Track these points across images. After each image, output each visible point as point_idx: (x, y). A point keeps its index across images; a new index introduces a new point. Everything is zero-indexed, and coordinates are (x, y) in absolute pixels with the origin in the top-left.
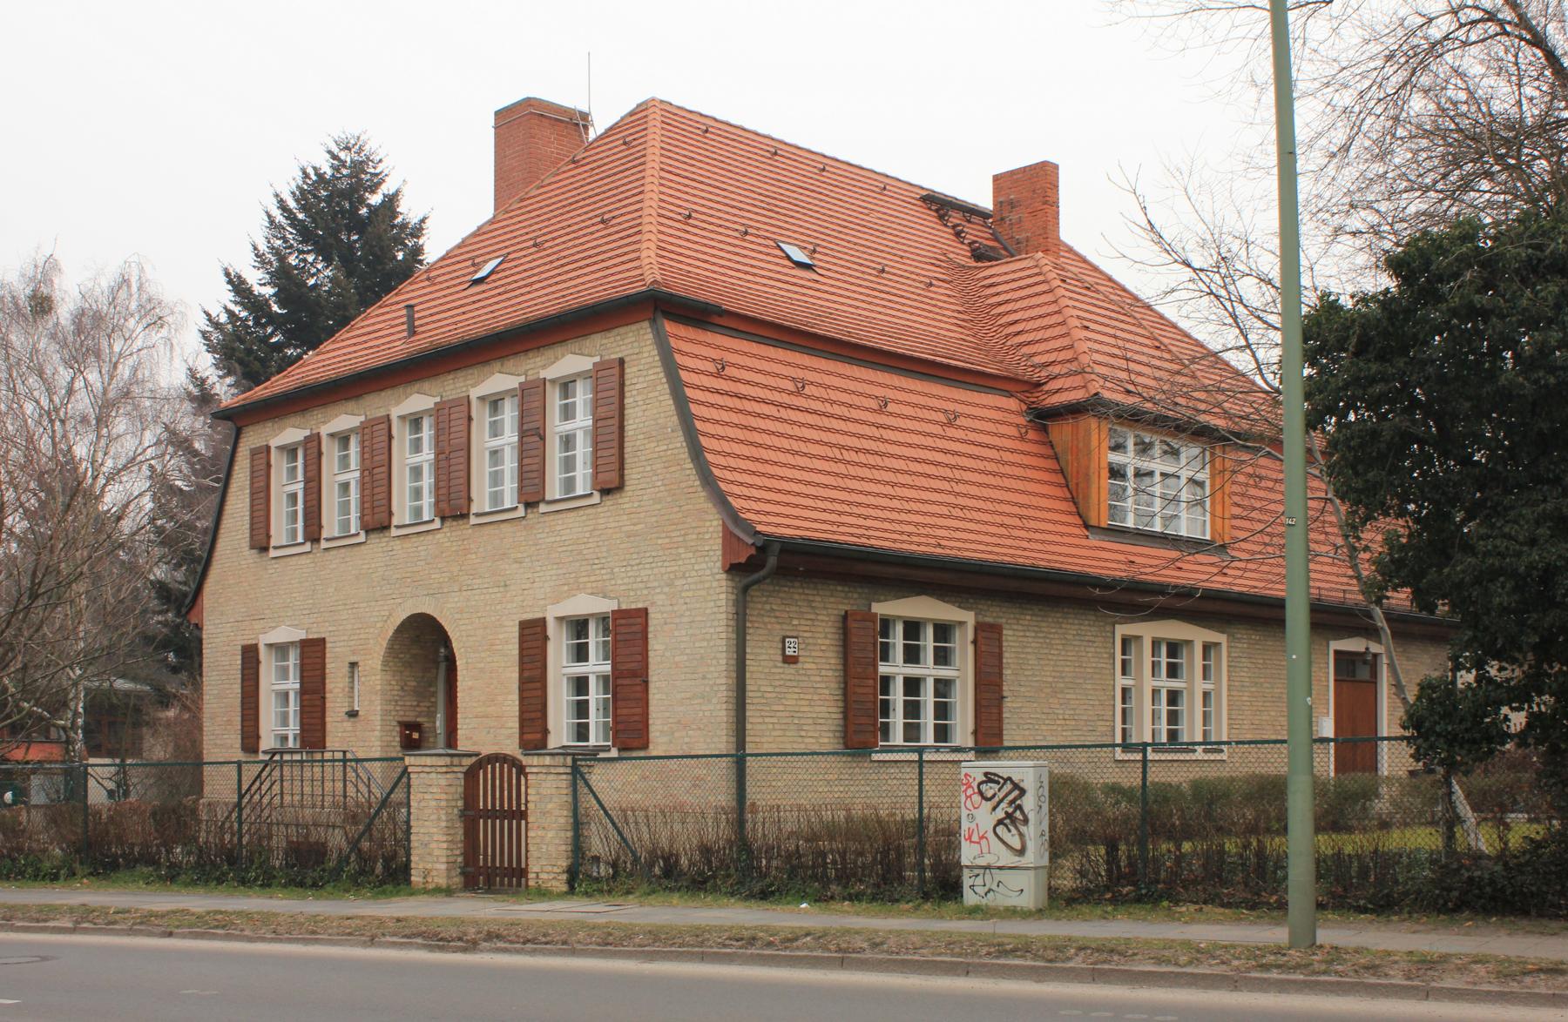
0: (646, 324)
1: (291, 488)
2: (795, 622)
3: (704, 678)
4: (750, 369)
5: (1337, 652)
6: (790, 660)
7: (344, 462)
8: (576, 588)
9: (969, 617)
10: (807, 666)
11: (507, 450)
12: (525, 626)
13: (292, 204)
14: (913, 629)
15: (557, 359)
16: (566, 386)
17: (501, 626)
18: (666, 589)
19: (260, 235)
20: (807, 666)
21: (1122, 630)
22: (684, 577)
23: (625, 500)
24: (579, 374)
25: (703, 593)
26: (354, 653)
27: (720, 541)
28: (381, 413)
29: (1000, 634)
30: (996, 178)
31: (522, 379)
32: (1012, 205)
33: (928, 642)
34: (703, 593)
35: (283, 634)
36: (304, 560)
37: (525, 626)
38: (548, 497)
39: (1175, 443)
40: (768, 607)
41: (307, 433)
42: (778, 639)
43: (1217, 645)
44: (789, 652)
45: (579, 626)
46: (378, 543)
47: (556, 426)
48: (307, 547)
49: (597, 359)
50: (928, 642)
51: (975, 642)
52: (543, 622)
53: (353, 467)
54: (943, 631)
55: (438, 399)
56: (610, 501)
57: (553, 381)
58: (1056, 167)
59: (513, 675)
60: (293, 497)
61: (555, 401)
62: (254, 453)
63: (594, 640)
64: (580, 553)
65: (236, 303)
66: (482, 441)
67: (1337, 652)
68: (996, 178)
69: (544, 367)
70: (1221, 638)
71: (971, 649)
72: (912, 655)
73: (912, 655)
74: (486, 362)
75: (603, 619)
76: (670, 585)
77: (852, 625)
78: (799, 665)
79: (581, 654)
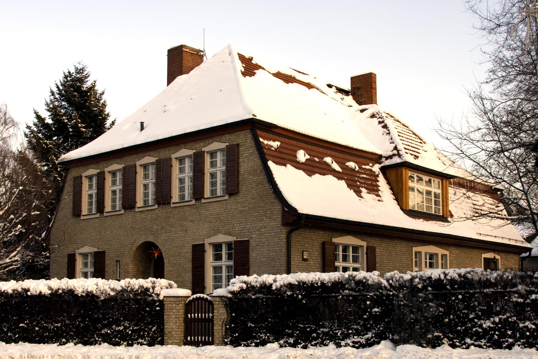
0: (248, 131)
1: (90, 192)
2: (307, 245)
3: (274, 267)
4: (286, 149)
5: (484, 258)
6: (305, 260)
7: (114, 183)
8: (217, 232)
9: (364, 244)
10: (311, 262)
11: (187, 179)
12: (195, 247)
13: (61, 88)
14: (345, 248)
15: (209, 144)
16: (213, 154)
17: (184, 247)
18: (257, 233)
19: (48, 97)
20: (311, 262)
21: (415, 249)
22: (265, 228)
23: (239, 198)
24: (219, 150)
25: (274, 234)
26: (118, 257)
27: (280, 214)
28: (132, 163)
29: (375, 251)
30: (352, 79)
31: (195, 151)
32: (358, 88)
33: (351, 254)
34: (274, 234)
35: (86, 249)
36: (96, 221)
37: (195, 247)
38: (205, 197)
39: (420, 176)
40: (297, 240)
41: (99, 171)
42: (301, 252)
43: (446, 255)
44: (305, 257)
45: (217, 247)
46: (129, 215)
47: (208, 169)
48: (98, 215)
49: (228, 144)
50: (351, 254)
51: (367, 253)
52: (203, 245)
53: (118, 184)
54: (356, 249)
55: (157, 158)
56: (233, 198)
57: (207, 152)
58: (375, 75)
59: (189, 266)
60: (91, 196)
61: (208, 159)
62: (75, 179)
63: (224, 253)
64: (219, 218)
65: (35, 124)
66: (176, 174)
67: (484, 258)
68: (352, 79)
69: (204, 147)
70: (447, 253)
71: (365, 256)
72: (345, 259)
73: (345, 259)
74: (178, 145)
75: (229, 245)
76: (259, 230)
77: (327, 246)
78: (308, 262)
79: (218, 257)
